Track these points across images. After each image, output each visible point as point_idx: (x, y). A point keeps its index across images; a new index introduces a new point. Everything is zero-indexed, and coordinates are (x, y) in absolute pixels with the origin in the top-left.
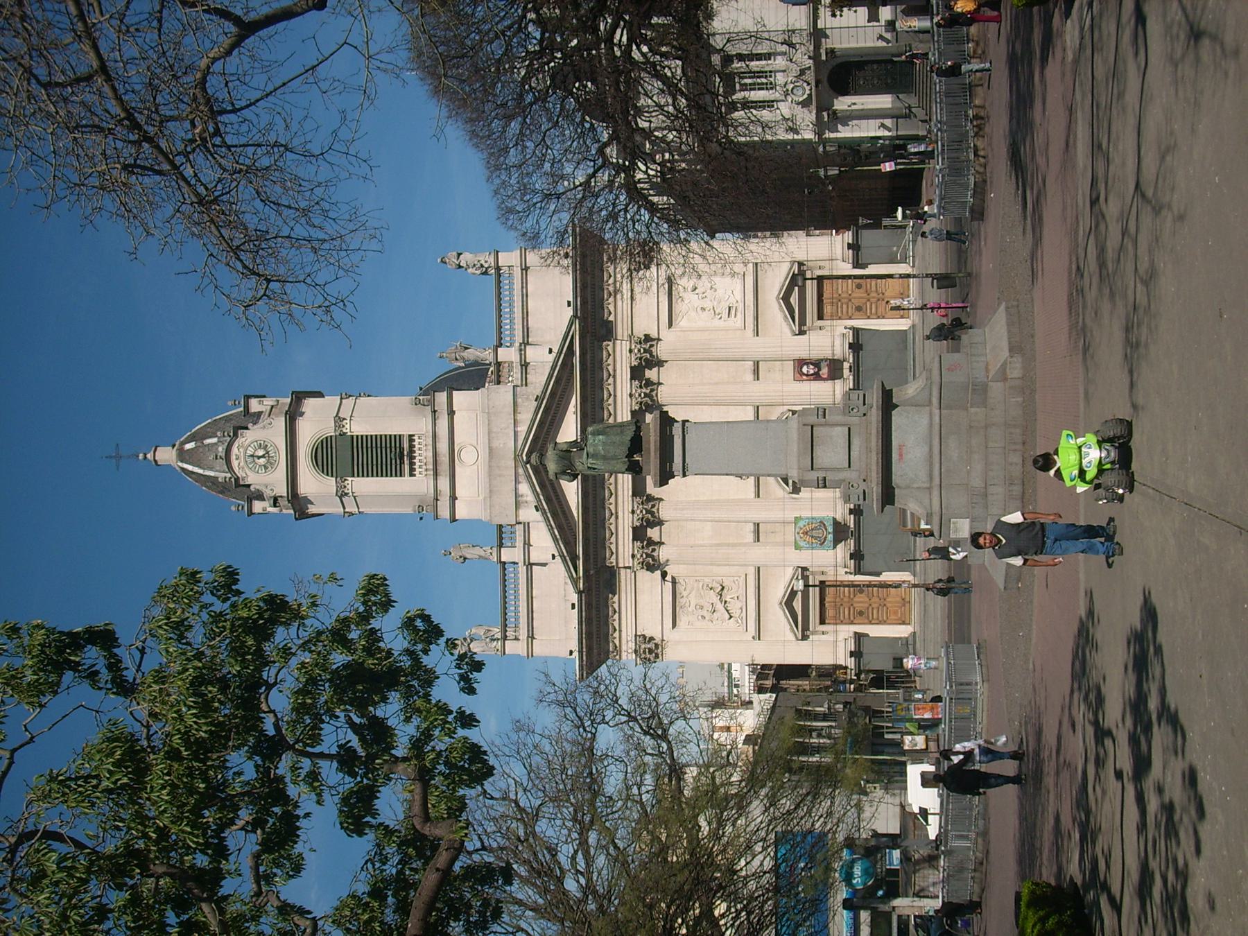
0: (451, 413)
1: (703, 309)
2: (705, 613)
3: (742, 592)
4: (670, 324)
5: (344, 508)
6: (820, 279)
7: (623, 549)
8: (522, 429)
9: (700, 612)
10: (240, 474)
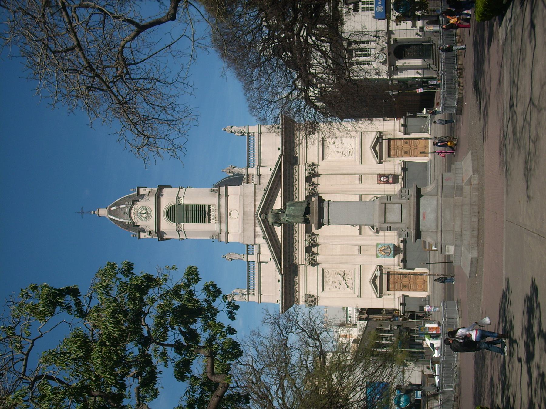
0: (227, 196)
1: (338, 152)
2: (336, 285)
3: (353, 276)
4: (323, 158)
5: (180, 236)
6: (389, 140)
7: (301, 256)
8: (258, 203)
9: (334, 285)
10: (135, 221)
